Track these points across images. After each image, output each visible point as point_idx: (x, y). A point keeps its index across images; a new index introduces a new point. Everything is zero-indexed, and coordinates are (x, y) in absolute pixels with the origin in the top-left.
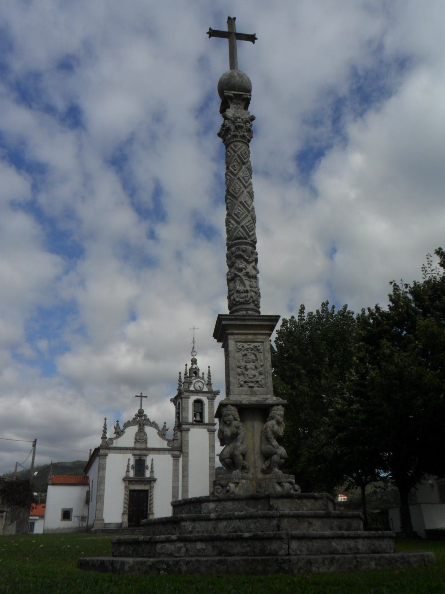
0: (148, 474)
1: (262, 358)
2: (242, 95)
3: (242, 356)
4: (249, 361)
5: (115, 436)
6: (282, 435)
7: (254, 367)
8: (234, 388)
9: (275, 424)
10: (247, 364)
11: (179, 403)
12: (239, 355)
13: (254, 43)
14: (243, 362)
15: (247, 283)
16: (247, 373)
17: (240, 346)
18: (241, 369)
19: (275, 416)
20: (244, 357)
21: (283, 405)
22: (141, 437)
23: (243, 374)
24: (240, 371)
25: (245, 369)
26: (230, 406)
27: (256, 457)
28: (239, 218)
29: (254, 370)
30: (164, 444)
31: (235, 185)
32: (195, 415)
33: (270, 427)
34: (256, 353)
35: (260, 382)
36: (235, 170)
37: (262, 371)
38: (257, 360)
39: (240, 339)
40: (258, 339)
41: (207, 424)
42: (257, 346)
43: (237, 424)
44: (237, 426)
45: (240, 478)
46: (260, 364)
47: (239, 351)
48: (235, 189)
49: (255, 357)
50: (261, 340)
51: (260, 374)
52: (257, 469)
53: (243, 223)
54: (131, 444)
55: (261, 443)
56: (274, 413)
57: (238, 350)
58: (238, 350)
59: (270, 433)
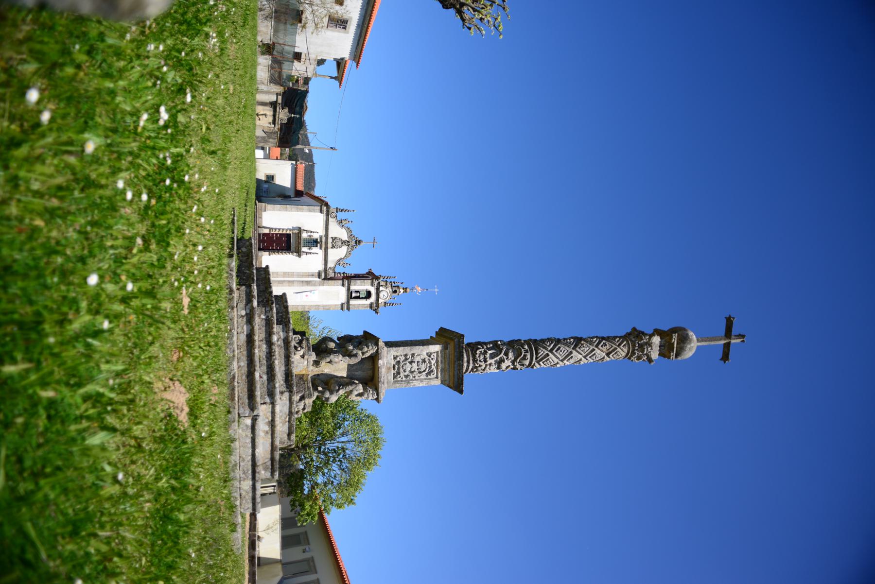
0: (305, 249)
1: (422, 377)
2: (673, 351)
5: (339, 219)
7: (413, 370)
8: (394, 351)
10: (416, 363)
11: (368, 277)
12: (425, 356)
13: (721, 360)
15: (493, 361)
16: (408, 364)
22: (337, 243)
23: (406, 359)
28: (556, 351)
30: (331, 264)
31: (588, 346)
32: (357, 292)
36: (602, 346)
38: (420, 373)
41: (348, 302)
48: (584, 347)
51: (407, 376)
53: (551, 355)
54: (331, 234)
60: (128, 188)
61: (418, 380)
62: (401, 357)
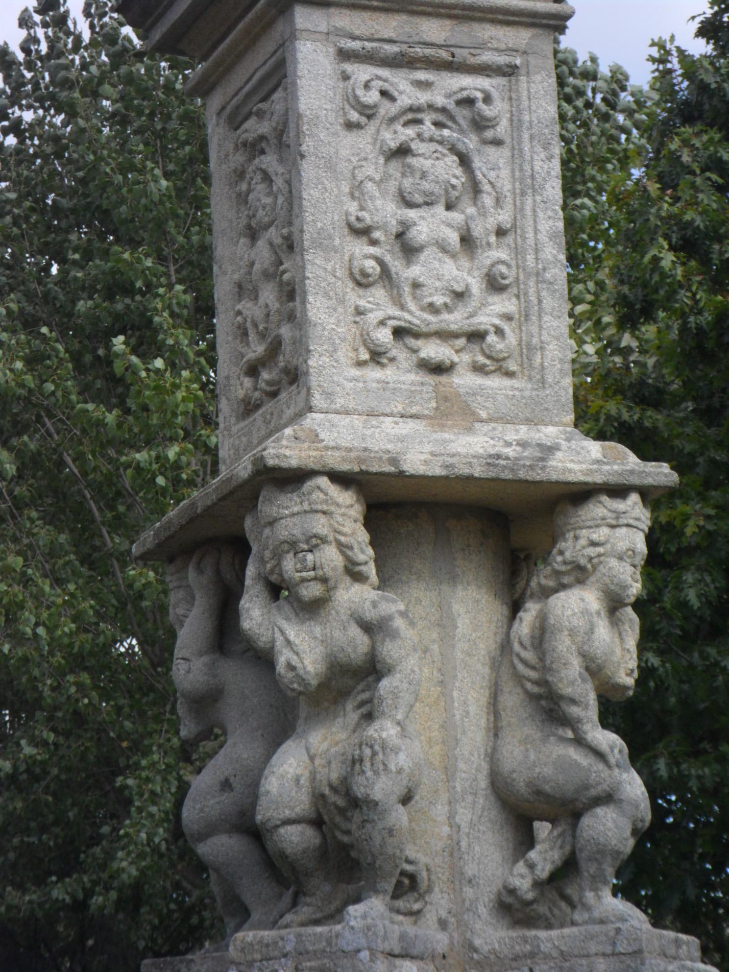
1: (504, 180)
3: (382, 161)
4: (425, 193)
6: (630, 681)
7: (453, 238)
9: (598, 613)
10: (412, 214)
14: (384, 194)
16: (415, 271)
17: (367, 86)
18: (374, 243)
19: (595, 563)
20: (395, 167)
21: (646, 493)
24: (367, 257)
25: (397, 248)
26: (323, 481)
27: (464, 816)
29: (453, 256)
33: (572, 633)
34: (470, 142)
35: (491, 338)
37: (509, 266)
38: (476, 190)
39: (370, 40)
40: (482, 46)
42: (479, 95)
43: (375, 604)
44: (370, 614)
45: (397, 951)
46: (491, 223)
47: (363, 120)
49: (459, 171)
50: (501, 60)
52: (469, 892)
55: (495, 731)
56: (593, 544)
57: (354, 116)
58: (354, 116)
59: (575, 667)
60: (89, 75)
61: (519, 210)
62: (373, 317)
